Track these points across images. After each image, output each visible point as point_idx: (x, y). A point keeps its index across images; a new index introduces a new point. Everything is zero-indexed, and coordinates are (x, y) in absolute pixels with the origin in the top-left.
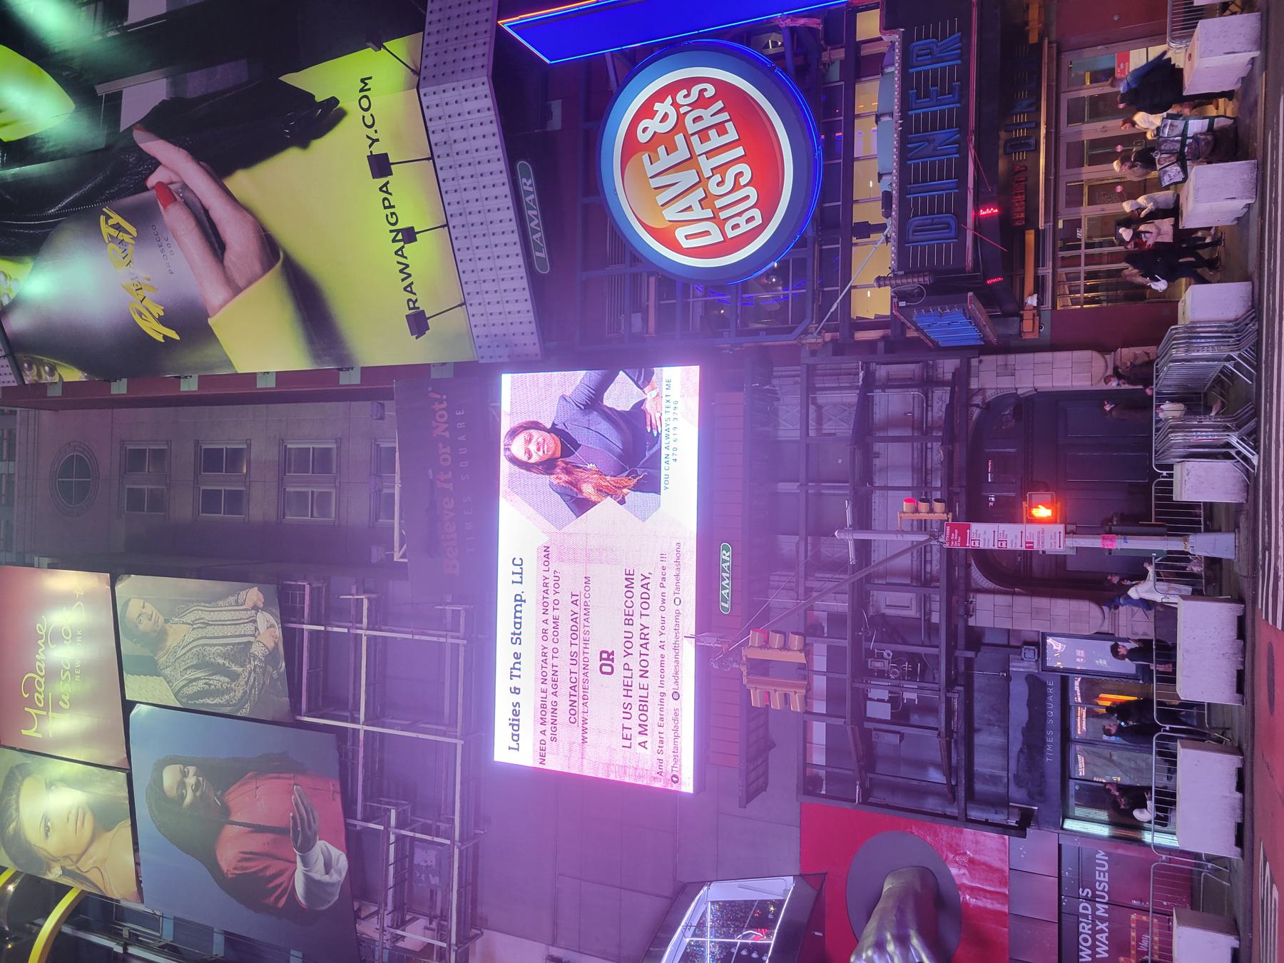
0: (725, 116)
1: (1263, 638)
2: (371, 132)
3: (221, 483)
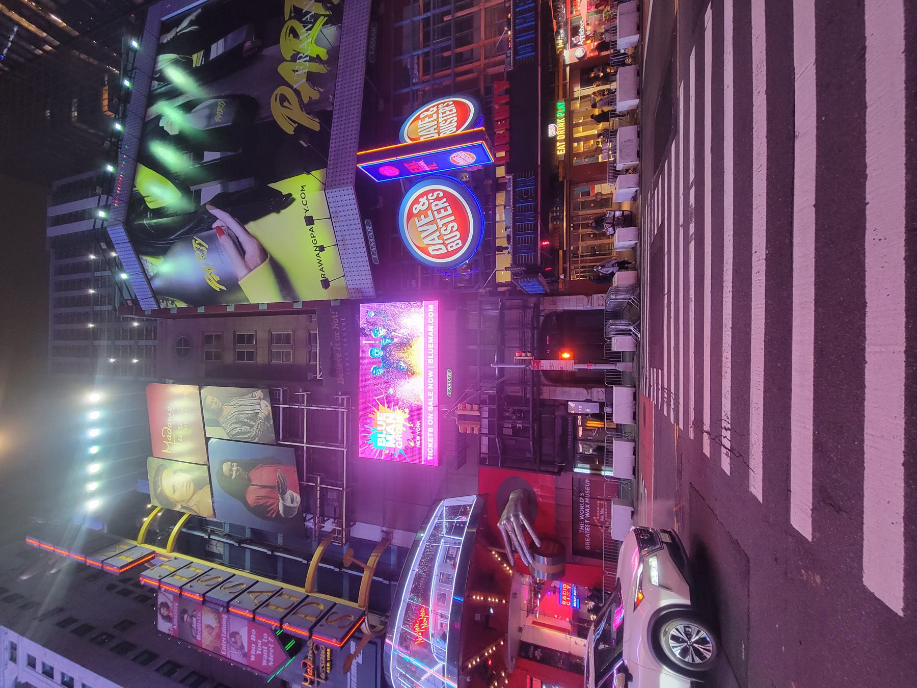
0: (447, 204)
1: (642, 400)
2: (305, 207)
3: (245, 348)
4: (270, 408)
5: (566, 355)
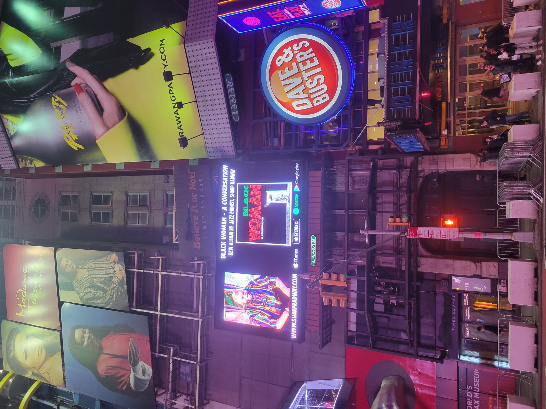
0: (313, 55)
2: (164, 62)
3: (101, 209)
4: (124, 272)
5: (449, 222)
